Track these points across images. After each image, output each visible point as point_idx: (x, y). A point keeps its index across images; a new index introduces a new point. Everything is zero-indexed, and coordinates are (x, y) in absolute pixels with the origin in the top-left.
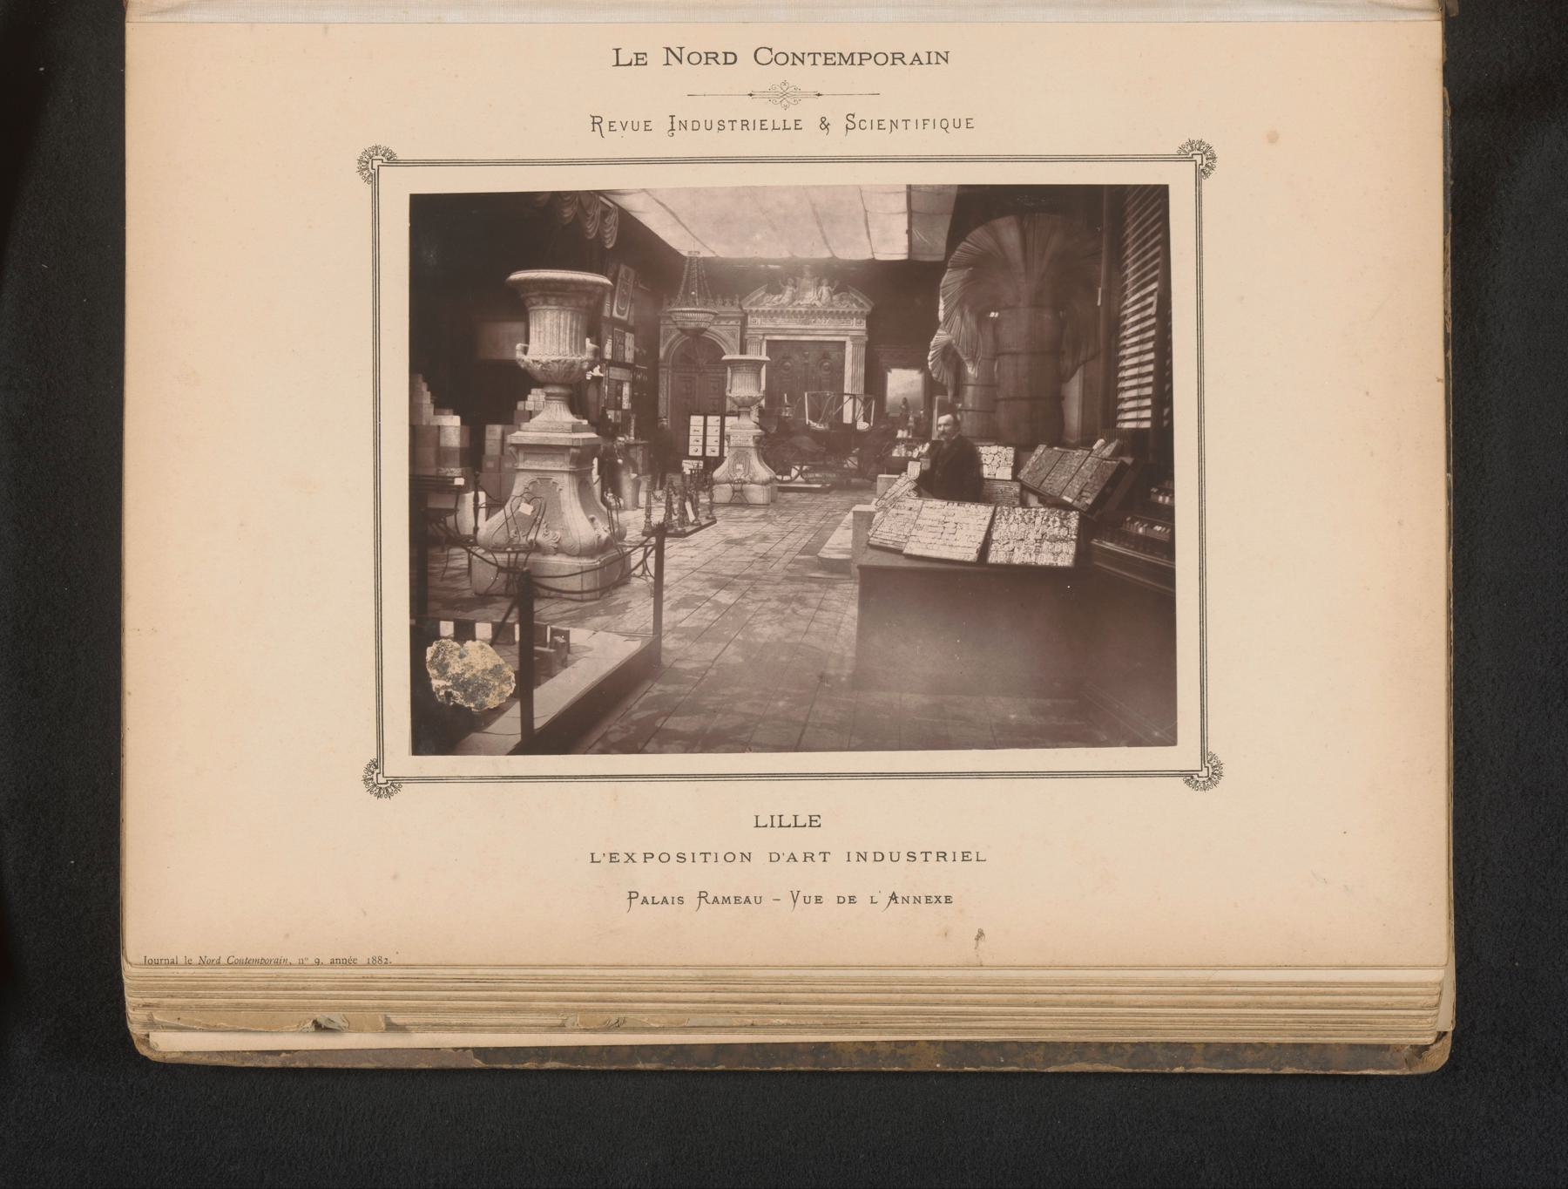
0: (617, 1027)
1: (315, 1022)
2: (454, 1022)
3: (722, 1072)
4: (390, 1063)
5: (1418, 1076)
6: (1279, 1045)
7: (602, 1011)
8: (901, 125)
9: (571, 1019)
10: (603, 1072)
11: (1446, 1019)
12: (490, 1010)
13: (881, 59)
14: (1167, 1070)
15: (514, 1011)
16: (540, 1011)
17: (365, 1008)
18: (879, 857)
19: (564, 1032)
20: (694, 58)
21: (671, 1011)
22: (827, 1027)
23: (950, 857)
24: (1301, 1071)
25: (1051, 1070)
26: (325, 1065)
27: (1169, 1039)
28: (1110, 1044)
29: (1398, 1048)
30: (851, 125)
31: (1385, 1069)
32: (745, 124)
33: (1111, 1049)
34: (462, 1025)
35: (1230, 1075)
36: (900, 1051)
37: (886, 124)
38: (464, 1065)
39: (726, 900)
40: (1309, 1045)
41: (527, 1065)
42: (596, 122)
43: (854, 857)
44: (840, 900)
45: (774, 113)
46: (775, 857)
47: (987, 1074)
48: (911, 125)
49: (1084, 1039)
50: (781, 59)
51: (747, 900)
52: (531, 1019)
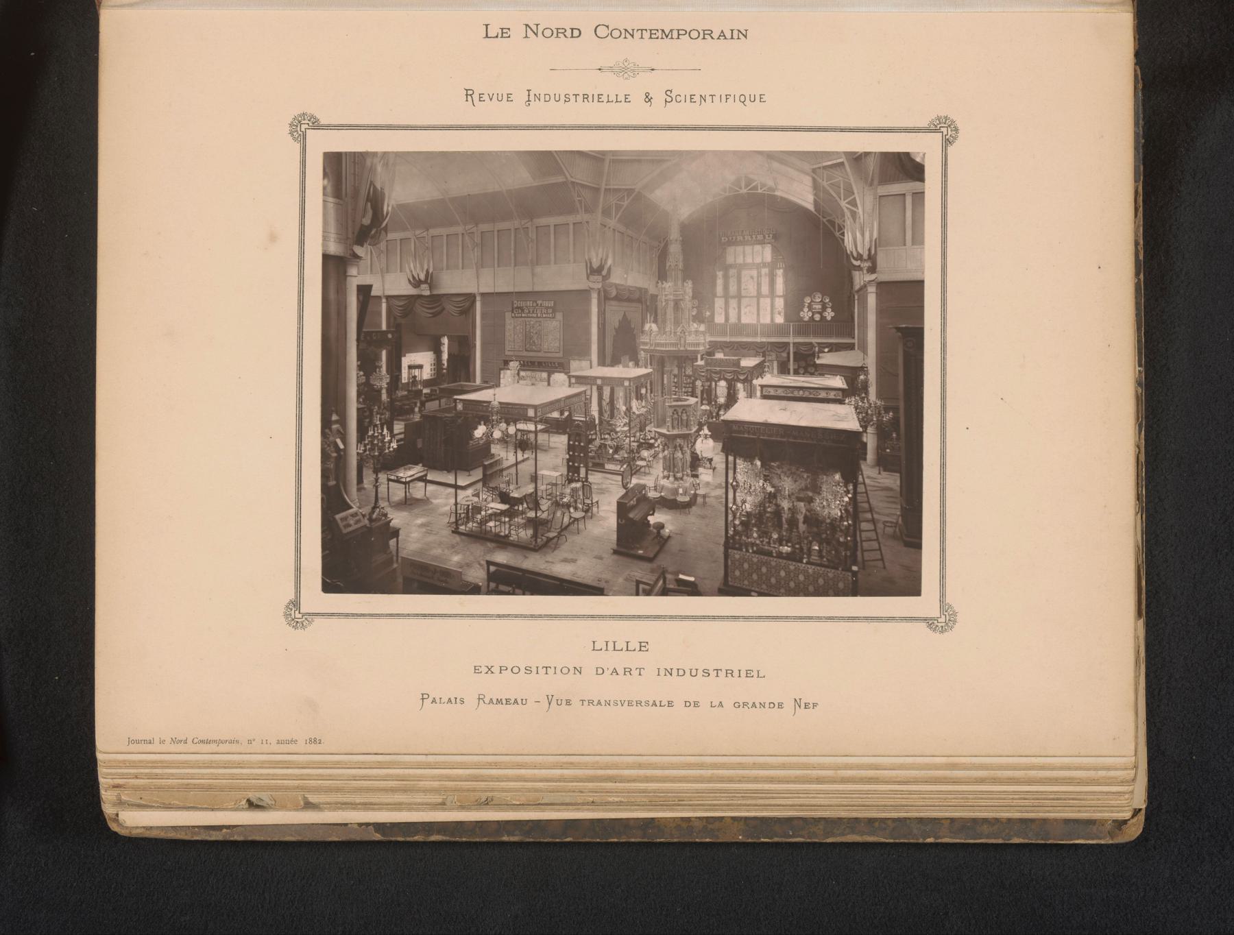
0: (487, 804)
1: (248, 801)
2: (358, 801)
3: (569, 843)
4: (308, 837)
5: (1117, 846)
6: (1009, 820)
7: (474, 790)
8: (709, 99)
9: (450, 798)
10: (476, 843)
11: (1138, 796)
12: (385, 790)
13: (694, 34)
14: (921, 841)
15: (405, 790)
16: (426, 791)
17: (287, 788)
18: (681, 672)
19: (444, 810)
20: (548, 33)
21: (529, 790)
22: (652, 805)
23: (736, 674)
24: (1026, 841)
25: (830, 840)
26: (258, 838)
27: (922, 815)
28: (875, 820)
29: (1102, 822)
30: (669, 99)
31: (1093, 839)
32: (585, 97)
33: (877, 824)
34: (365, 804)
35: (969, 844)
36: (710, 826)
37: (697, 98)
38: (367, 838)
39: (499, 701)
40: (1032, 820)
41: (416, 838)
42: (469, 94)
43: (662, 673)
44: (687, 704)
45: (610, 85)
46: (600, 671)
47: (777, 844)
48: (716, 99)
49: (854, 815)
50: (616, 34)
51: (516, 701)
52: (419, 798)
